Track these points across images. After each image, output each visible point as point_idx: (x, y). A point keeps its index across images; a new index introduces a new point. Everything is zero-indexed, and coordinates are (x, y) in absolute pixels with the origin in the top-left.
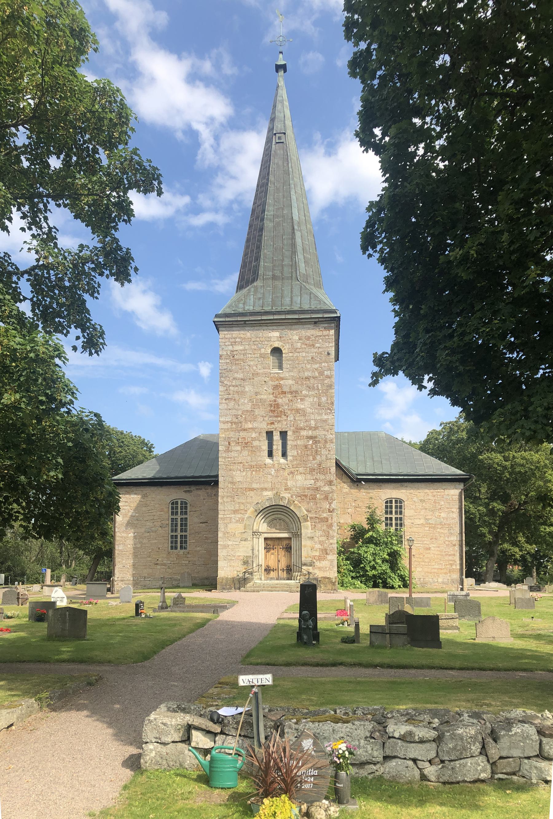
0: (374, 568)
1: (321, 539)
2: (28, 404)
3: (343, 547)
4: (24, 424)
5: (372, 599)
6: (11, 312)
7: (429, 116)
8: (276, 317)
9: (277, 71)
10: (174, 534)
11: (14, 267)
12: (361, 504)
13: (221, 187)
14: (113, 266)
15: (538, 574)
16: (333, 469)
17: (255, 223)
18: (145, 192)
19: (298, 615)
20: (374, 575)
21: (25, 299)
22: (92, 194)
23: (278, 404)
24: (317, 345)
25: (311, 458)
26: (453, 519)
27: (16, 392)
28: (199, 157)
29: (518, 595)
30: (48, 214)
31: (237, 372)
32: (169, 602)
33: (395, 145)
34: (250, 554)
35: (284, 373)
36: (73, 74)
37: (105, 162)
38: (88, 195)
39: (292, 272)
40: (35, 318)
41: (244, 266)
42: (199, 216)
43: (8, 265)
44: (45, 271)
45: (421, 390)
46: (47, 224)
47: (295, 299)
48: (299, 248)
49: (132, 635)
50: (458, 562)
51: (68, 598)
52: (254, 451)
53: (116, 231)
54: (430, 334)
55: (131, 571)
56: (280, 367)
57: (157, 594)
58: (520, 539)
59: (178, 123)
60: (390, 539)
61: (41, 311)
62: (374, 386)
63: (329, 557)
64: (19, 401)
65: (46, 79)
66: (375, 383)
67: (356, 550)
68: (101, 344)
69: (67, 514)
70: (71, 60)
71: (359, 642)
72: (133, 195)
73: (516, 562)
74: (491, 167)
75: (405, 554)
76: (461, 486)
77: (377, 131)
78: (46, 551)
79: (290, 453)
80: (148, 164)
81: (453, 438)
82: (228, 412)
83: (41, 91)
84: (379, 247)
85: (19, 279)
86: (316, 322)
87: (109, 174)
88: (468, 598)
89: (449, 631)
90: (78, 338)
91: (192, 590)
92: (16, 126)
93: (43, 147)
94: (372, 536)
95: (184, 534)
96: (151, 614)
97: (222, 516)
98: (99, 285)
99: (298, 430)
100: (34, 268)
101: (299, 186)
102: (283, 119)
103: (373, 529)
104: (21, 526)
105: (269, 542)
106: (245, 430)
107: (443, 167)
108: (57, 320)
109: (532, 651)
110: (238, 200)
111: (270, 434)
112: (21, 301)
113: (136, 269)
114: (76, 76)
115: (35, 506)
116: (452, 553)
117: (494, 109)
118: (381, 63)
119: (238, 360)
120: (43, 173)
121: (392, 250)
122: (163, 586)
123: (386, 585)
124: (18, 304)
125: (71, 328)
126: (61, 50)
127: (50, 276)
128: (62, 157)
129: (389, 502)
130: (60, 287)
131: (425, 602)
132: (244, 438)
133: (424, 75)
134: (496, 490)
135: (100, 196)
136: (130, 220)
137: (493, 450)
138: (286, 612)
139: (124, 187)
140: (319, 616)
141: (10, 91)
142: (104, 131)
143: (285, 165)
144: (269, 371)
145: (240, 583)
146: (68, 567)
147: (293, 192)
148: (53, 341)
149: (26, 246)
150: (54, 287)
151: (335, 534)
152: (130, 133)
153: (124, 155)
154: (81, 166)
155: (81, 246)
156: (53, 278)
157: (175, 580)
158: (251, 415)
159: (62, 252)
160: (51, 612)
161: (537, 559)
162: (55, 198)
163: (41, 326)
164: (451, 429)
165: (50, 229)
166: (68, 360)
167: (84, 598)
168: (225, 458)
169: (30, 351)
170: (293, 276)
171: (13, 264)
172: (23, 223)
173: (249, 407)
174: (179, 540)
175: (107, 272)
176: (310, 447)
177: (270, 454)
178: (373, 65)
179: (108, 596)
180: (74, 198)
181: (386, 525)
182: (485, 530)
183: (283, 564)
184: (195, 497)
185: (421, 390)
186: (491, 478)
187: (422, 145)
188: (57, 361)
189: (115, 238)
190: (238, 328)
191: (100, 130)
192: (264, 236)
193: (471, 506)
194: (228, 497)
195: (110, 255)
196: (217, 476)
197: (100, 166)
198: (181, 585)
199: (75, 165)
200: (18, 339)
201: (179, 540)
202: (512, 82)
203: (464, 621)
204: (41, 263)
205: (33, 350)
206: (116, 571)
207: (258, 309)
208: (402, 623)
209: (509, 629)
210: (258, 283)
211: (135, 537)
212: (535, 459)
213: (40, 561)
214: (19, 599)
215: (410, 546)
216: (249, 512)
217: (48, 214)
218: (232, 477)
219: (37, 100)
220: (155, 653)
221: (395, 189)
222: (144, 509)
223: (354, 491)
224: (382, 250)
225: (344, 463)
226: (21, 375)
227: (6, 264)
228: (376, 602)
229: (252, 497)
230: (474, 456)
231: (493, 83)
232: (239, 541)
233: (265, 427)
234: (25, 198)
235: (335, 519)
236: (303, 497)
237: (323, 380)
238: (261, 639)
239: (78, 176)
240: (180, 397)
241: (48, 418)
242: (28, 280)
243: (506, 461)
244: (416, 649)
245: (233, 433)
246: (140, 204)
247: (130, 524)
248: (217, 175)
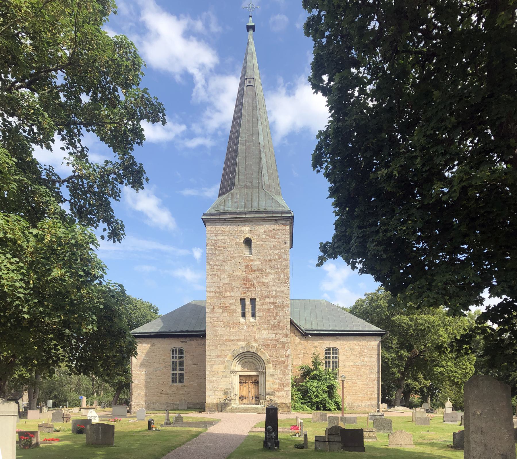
0: (317, 396)
1: (279, 376)
2: (71, 277)
3: (295, 382)
4: (67, 292)
5: (316, 418)
6: (56, 210)
7: (362, 67)
8: (247, 216)
9: (248, 31)
10: (174, 372)
11: (56, 177)
12: (308, 351)
13: (209, 118)
14: (130, 177)
15: (431, 401)
16: (289, 326)
17: (232, 146)
18: (153, 121)
19: (264, 429)
20: (317, 401)
21: (65, 200)
22: (114, 123)
23: (249, 279)
24: (277, 237)
25: (273, 318)
26: (373, 362)
27: (62, 268)
28: (194, 94)
29: (418, 415)
30: (81, 138)
31: (219, 256)
32: (172, 420)
33: (339, 89)
35: (253, 257)
36: (98, 31)
37: (122, 98)
38: (110, 123)
40: (73, 215)
41: (224, 178)
42: (192, 140)
43: (52, 175)
44: (80, 180)
45: (353, 270)
46: (80, 144)
47: (261, 203)
48: (264, 165)
49: (146, 443)
50: (376, 392)
51: (99, 417)
52: (232, 313)
53: (131, 151)
54: (362, 230)
55: (144, 398)
56: (251, 252)
57: (163, 415)
58: (419, 376)
59: (176, 69)
60: (328, 376)
61: (77, 210)
62: (319, 266)
63: (285, 389)
64: (64, 275)
65: (79, 34)
66: (320, 264)
67: (304, 384)
68: (122, 234)
69: (99, 357)
70: (96, 20)
71: (307, 448)
72: (144, 124)
73: (416, 392)
74: (408, 107)
75: (339, 386)
76: (379, 339)
77: (325, 78)
78: (82, 384)
80: (155, 101)
81: (374, 305)
82: (213, 284)
83: (75, 44)
84: (325, 165)
85: (60, 186)
86: (276, 220)
87: (126, 108)
88: (383, 417)
89: (371, 440)
90: (105, 230)
91: (188, 412)
92: (56, 70)
93: (75, 87)
94: (315, 374)
95: (181, 372)
96: (160, 428)
97: (209, 360)
98: (120, 191)
99: (263, 297)
100: (71, 178)
101: (264, 119)
102: (252, 67)
103: (316, 369)
104: (67, 366)
105: (242, 378)
106: (225, 297)
107: (372, 106)
108: (89, 216)
109: (429, 454)
110: (221, 128)
111: (243, 301)
112: (62, 202)
113: (147, 180)
114: (100, 33)
115: (77, 352)
116: (372, 386)
117: (409, 63)
118: (328, 26)
119: (220, 247)
120: (77, 106)
121: (334, 167)
122: (167, 408)
123: (325, 409)
124: (60, 204)
125: (99, 222)
126: (89, 13)
127: (83, 184)
128: (90, 94)
129: (328, 350)
130: (91, 192)
131: (353, 420)
132: (224, 303)
133: (361, 36)
134: (403, 342)
135: (119, 124)
136: (142, 143)
137: (402, 313)
138: (255, 427)
139: (137, 118)
140: (279, 430)
141: (51, 43)
142: (121, 75)
143: (254, 102)
144: (242, 255)
145: (222, 407)
146: (98, 395)
147: (259, 124)
148: (88, 232)
149: (66, 161)
150: (86, 192)
151: (290, 373)
152: (140, 76)
153: (137, 93)
154: (104, 101)
155: (106, 162)
156: (86, 185)
157: (175, 405)
159: (92, 166)
160: (88, 427)
161: (431, 390)
162: (86, 125)
163: (77, 221)
164: (373, 299)
165: (83, 148)
166: (99, 245)
167: (111, 417)
168: (210, 318)
169: (71, 239)
170: (260, 186)
171: (56, 175)
172: (63, 144)
173: (227, 281)
174: (178, 376)
175: (126, 181)
177: (243, 315)
178: (322, 27)
179: (128, 416)
180: (100, 125)
181: (326, 366)
182: (395, 370)
184: (189, 346)
185: (353, 270)
186: (400, 333)
187: (357, 89)
188: (91, 246)
189: (131, 156)
190: (220, 224)
191: (118, 73)
192: (237, 156)
193: (386, 353)
194: (213, 346)
195: (128, 169)
196: (205, 331)
197: (119, 101)
198: (179, 408)
199: (100, 100)
200: (62, 230)
201: (178, 376)
202: (423, 43)
203: (380, 433)
204: (77, 174)
205: (74, 237)
206: (133, 398)
207: (234, 210)
208: (338, 434)
209: (412, 439)
210: (234, 191)
211: (146, 374)
212: (431, 320)
213: (78, 391)
214: (64, 418)
215: (343, 381)
216: (228, 356)
217: (81, 138)
219: (71, 51)
220: (163, 455)
221: (338, 122)
222: (152, 354)
223: (303, 342)
224: (327, 167)
225: (296, 322)
226: (65, 256)
227: (51, 174)
228: (318, 420)
229: (230, 346)
230: (388, 318)
231: (409, 43)
232: (221, 377)
233: (240, 295)
234: (64, 125)
235: (290, 362)
236: (266, 346)
237: (282, 262)
238: (238, 446)
239: (103, 109)
240: (179, 273)
241: (85, 287)
242: (67, 187)
243: (411, 321)
244: (347, 452)
245: (216, 300)
246: (150, 130)
247: (142, 365)
248: (206, 110)
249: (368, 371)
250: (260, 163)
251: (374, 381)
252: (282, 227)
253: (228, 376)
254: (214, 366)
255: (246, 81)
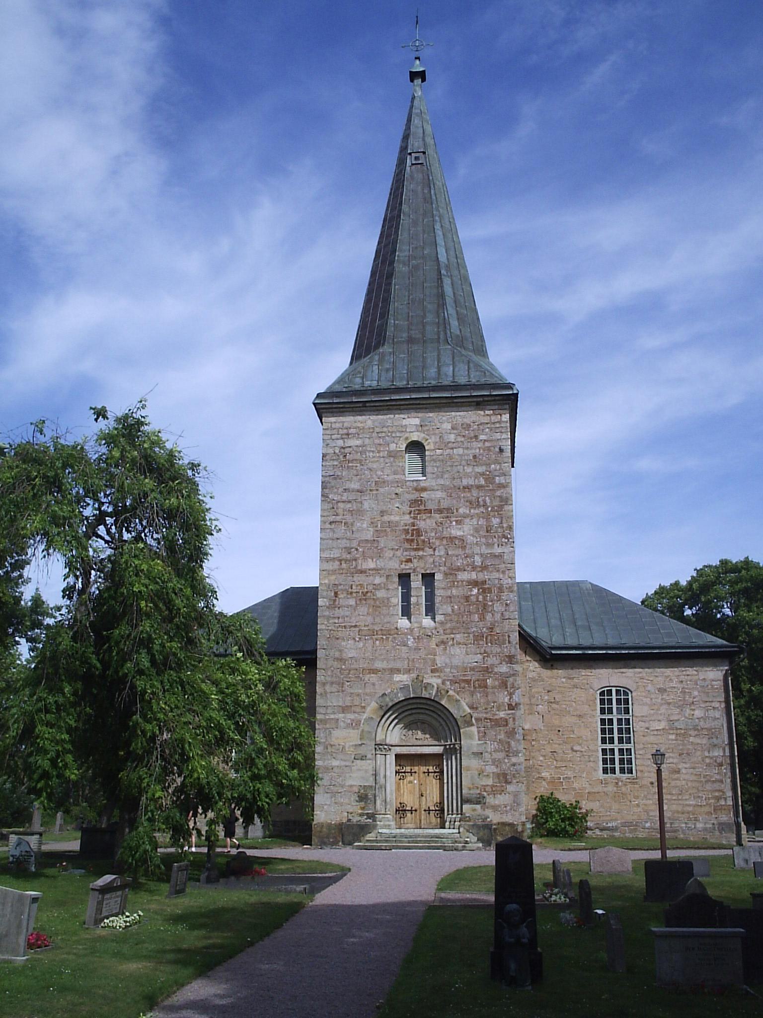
9: (412, 81)
16: (515, 637)
23: (418, 530)
24: (482, 437)
26: (715, 719)
31: (350, 480)
34: (371, 782)
39: (438, 333)
47: (444, 369)
48: (449, 300)
50: (729, 794)
52: (379, 606)
63: (510, 788)
79: (442, 608)
82: (335, 544)
86: (479, 403)
99: (452, 572)
101: (447, 220)
102: (421, 135)
106: (362, 572)
111: (404, 579)
116: (718, 777)
143: (426, 191)
147: (438, 226)
158: (373, 548)
168: (328, 618)
173: (369, 535)
176: (473, 599)
183: (432, 797)
194: (332, 683)
196: (315, 651)
207: (384, 384)
210: (386, 348)
216: (368, 709)
218: (340, 651)
223: (546, 673)
233: (397, 567)
236: (462, 683)
249: (704, 741)
250: (441, 296)
251: (721, 765)
252: (493, 418)
253: (369, 756)
254: (336, 733)
255: (409, 157)
